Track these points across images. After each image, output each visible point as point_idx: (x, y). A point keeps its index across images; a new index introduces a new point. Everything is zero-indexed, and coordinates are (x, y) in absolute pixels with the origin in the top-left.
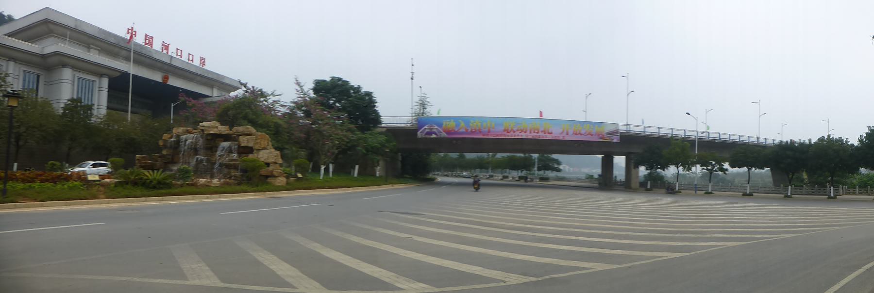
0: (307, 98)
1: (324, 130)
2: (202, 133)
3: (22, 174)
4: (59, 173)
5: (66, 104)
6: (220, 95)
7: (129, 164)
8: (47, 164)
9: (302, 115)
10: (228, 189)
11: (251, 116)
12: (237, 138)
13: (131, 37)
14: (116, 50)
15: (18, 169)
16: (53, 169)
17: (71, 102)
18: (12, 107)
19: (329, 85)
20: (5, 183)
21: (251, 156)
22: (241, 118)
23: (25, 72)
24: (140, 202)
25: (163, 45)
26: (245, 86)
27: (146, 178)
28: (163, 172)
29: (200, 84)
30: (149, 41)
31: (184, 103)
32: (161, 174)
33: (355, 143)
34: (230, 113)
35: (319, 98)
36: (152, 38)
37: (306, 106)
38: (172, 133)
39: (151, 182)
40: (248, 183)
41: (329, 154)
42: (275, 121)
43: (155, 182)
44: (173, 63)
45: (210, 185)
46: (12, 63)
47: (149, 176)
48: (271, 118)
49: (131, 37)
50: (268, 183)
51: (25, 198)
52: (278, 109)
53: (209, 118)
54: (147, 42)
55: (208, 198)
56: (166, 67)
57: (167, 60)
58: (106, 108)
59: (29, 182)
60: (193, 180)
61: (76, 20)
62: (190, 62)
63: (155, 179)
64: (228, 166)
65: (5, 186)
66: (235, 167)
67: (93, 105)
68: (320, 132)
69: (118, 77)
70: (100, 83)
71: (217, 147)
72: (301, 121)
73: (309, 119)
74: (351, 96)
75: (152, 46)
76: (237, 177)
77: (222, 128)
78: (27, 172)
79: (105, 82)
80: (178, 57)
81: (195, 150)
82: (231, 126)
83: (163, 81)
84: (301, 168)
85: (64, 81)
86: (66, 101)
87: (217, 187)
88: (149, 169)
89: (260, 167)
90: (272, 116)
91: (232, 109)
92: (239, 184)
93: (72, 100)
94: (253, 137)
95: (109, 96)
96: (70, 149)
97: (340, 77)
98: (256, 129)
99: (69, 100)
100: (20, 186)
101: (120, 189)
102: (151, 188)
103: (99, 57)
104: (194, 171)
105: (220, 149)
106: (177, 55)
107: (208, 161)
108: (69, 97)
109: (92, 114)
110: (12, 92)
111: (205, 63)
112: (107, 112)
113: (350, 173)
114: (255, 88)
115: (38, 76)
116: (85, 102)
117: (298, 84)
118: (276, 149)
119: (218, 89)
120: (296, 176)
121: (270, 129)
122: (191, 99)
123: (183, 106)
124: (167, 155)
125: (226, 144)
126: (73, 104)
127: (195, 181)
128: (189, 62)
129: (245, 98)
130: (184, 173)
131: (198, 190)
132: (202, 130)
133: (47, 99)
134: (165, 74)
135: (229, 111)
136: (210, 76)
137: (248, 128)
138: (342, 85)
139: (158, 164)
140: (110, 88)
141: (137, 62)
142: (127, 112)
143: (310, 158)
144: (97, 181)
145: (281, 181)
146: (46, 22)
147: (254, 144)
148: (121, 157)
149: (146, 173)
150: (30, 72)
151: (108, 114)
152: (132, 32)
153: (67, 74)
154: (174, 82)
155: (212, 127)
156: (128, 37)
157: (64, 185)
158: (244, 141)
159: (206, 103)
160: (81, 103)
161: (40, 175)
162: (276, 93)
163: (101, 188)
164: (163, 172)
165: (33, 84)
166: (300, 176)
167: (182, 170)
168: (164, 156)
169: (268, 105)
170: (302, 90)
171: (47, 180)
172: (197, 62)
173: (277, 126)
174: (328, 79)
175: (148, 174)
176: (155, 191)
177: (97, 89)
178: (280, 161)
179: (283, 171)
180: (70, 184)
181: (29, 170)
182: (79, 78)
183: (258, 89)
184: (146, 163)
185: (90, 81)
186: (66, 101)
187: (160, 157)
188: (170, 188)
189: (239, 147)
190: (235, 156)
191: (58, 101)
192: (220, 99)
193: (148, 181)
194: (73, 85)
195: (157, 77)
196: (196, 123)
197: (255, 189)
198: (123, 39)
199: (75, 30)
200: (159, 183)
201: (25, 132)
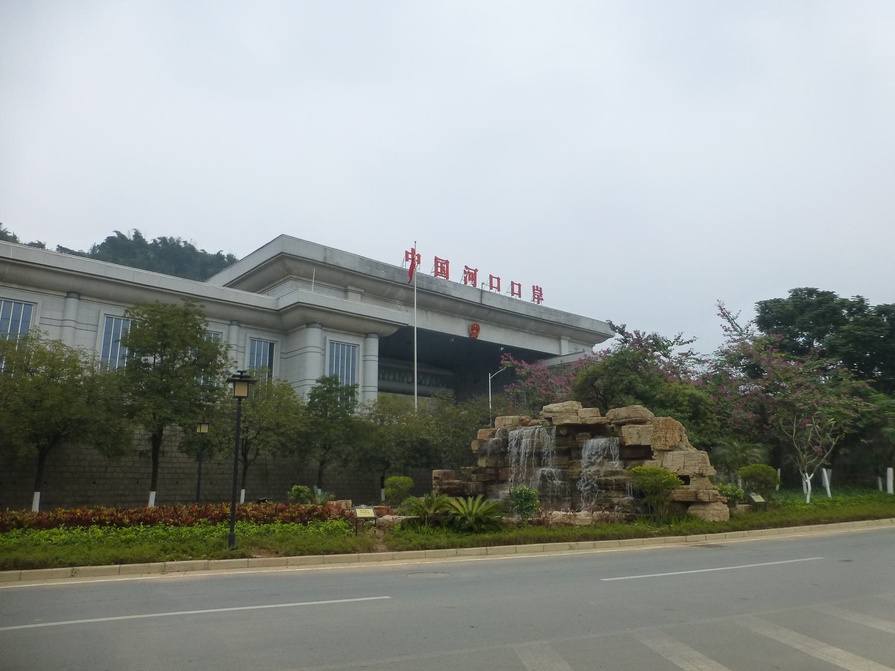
0: (747, 341)
1: (798, 400)
2: (548, 423)
3: (255, 509)
4: (310, 506)
5: (313, 388)
6: (574, 351)
7: (421, 488)
8: (290, 490)
9: (742, 375)
10: (610, 530)
11: (640, 387)
12: (615, 430)
13: (413, 266)
14: (389, 289)
15: (246, 500)
16: (299, 499)
17: (322, 383)
18: (240, 398)
19: (790, 308)
20: (232, 525)
21: (648, 465)
22: (621, 391)
23: (253, 340)
24: (448, 556)
25: (465, 272)
26: (622, 332)
27: (455, 512)
28: (483, 500)
29: (537, 335)
30: (442, 268)
31: (511, 371)
32: (480, 504)
33: (876, 420)
34: (599, 383)
35: (773, 338)
36: (447, 262)
37: (749, 356)
38: (494, 426)
39: (464, 519)
40: (648, 518)
41: (817, 449)
42: (688, 392)
43: (471, 519)
44: (487, 302)
45: (572, 522)
46: (234, 329)
47: (460, 508)
48: (681, 387)
49: (413, 266)
50: (691, 517)
51: (262, 550)
52: (691, 368)
53: (559, 395)
54: (439, 270)
55: (571, 548)
56: (474, 311)
57: (475, 298)
58: (376, 389)
59: (265, 522)
60: (540, 514)
61: (325, 248)
62: (515, 297)
63: (470, 514)
64: (604, 486)
65: (232, 530)
66: (620, 487)
67: (355, 386)
68: (789, 406)
69: (395, 333)
70: (365, 346)
71: (579, 449)
72: (742, 388)
73: (760, 381)
74: (846, 322)
75: (447, 277)
76: (623, 506)
77: (585, 412)
78: (262, 505)
79: (374, 345)
80: (494, 290)
81: (537, 456)
82: (604, 409)
83: (471, 335)
84: (763, 485)
85: (309, 349)
86: (314, 382)
87: (588, 526)
88: (459, 496)
89: (670, 485)
90: (681, 384)
91: (602, 375)
92: (630, 520)
93: (323, 380)
94: (649, 427)
95: (380, 368)
96: (322, 463)
97: (810, 286)
98: (652, 411)
99: (318, 381)
100: (253, 529)
101: (411, 533)
102: (464, 530)
103: (363, 304)
104: (540, 496)
105: (585, 454)
106: (491, 287)
107: (564, 477)
108: (318, 376)
109: (355, 402)
110: (239, 374)
111: (543, 297)
112: (379, 397)
113: (875, 486)
114: (641, 334)
115: (272, 345)
116: (344, 382)
117: (725, 315)
118: (698, 447)
119: (569, 341)
120: (750, 501)
121: (682, 408)
122: (524, 363)
123: (511, 376)
124: (487, 467)
125: (600, 442)
126: (324, 387)
127: (543, 515)
128: (514, 297)
129: (622, 353)
130: (523, 502)
131: (551, 534)
132: (550, 419)
133: (285, 381)
134: (471, 323)
135: (596, 379)
136: (553, 318)
137: (636, 410)
138: (820, 303)
139: (472, 485)
140: (382, 354)
141: (424, 306)
142: (413, 394)
143: (775, 459)
144: (371, 518)
145: (718, 511)
146: (282, 257)
147: (651, 440)
148: (405, 474)
149: (454, 502)
150: (260, 340)
151: (381, 401)
152: (413, 257)
153: (314, 337)
154: (489, 335)
155: (567, 411)
156: (408, 265)
157: (318, 527)
158: (632, 436)
159: (551, 368)
160: (337, 383)
161: (282, 510)
162: (685, 338)
163: (379, 533)
164: (483, 500)
165: (264, 360)
166: (758, 499)
167: (519, 496)
168: (481, 470)
169: (671, 363)
170: (735, 327)
171: (293, 519)
172: (527, 296)
173: (695, 402)
174: (785, 296)
175: (459, 506)
176: (473, 536)
177: (361, 358)
178: (711, 471)
179: (720, 492)
180: (329, 524)
181: (264, 501)
182: (332, 343)
183: (646, 336)
184: (451, 484)
185: (349, 345)
186: (314, 382)
187: (474, 472)
188: (499, 530)
189: (622, 446)
190: (616, 465)
191: (300, 384)
192: (575, 358)
193: (459, 517)
194: (324, 355)
195: (459, 329)
196: (536, 407)
197: (665, 528)
198: (399, 270)
199: (324, 266)
200: (479, 520)
201: (255, 438)
